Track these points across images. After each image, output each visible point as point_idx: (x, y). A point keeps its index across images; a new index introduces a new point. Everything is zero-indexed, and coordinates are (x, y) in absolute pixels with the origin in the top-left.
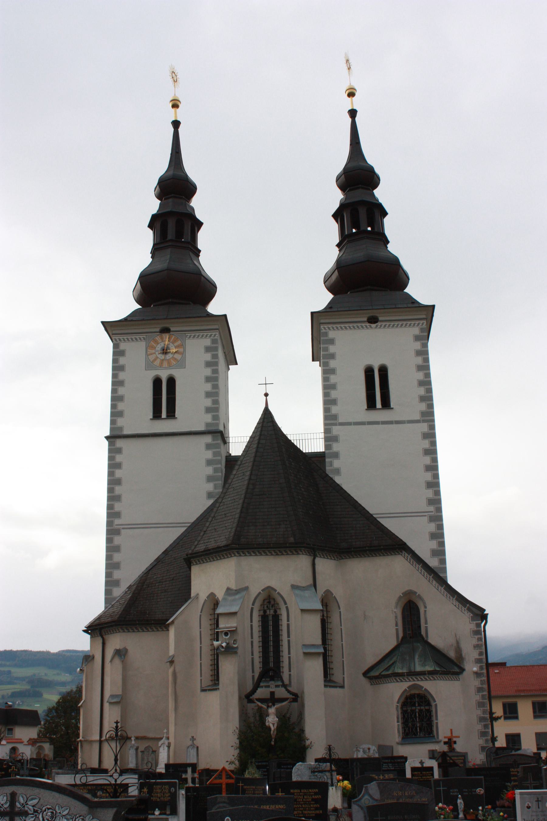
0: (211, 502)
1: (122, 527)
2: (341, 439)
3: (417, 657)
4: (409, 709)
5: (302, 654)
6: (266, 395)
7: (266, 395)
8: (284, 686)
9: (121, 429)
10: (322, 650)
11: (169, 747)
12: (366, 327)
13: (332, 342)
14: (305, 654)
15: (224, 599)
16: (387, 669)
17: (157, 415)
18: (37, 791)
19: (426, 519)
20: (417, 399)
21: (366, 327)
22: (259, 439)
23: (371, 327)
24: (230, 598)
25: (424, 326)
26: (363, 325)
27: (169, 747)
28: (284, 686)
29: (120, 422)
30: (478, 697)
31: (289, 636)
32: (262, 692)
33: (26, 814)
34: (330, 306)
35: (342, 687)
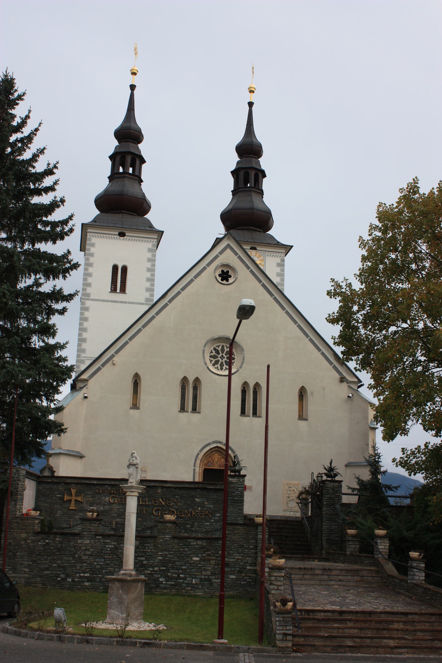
1: (86, 358)
12: (117, 238)
13: (93, 245)
21: (117, 238)
23: (120, 239)
26: (115, 237)
34: (95, 220)
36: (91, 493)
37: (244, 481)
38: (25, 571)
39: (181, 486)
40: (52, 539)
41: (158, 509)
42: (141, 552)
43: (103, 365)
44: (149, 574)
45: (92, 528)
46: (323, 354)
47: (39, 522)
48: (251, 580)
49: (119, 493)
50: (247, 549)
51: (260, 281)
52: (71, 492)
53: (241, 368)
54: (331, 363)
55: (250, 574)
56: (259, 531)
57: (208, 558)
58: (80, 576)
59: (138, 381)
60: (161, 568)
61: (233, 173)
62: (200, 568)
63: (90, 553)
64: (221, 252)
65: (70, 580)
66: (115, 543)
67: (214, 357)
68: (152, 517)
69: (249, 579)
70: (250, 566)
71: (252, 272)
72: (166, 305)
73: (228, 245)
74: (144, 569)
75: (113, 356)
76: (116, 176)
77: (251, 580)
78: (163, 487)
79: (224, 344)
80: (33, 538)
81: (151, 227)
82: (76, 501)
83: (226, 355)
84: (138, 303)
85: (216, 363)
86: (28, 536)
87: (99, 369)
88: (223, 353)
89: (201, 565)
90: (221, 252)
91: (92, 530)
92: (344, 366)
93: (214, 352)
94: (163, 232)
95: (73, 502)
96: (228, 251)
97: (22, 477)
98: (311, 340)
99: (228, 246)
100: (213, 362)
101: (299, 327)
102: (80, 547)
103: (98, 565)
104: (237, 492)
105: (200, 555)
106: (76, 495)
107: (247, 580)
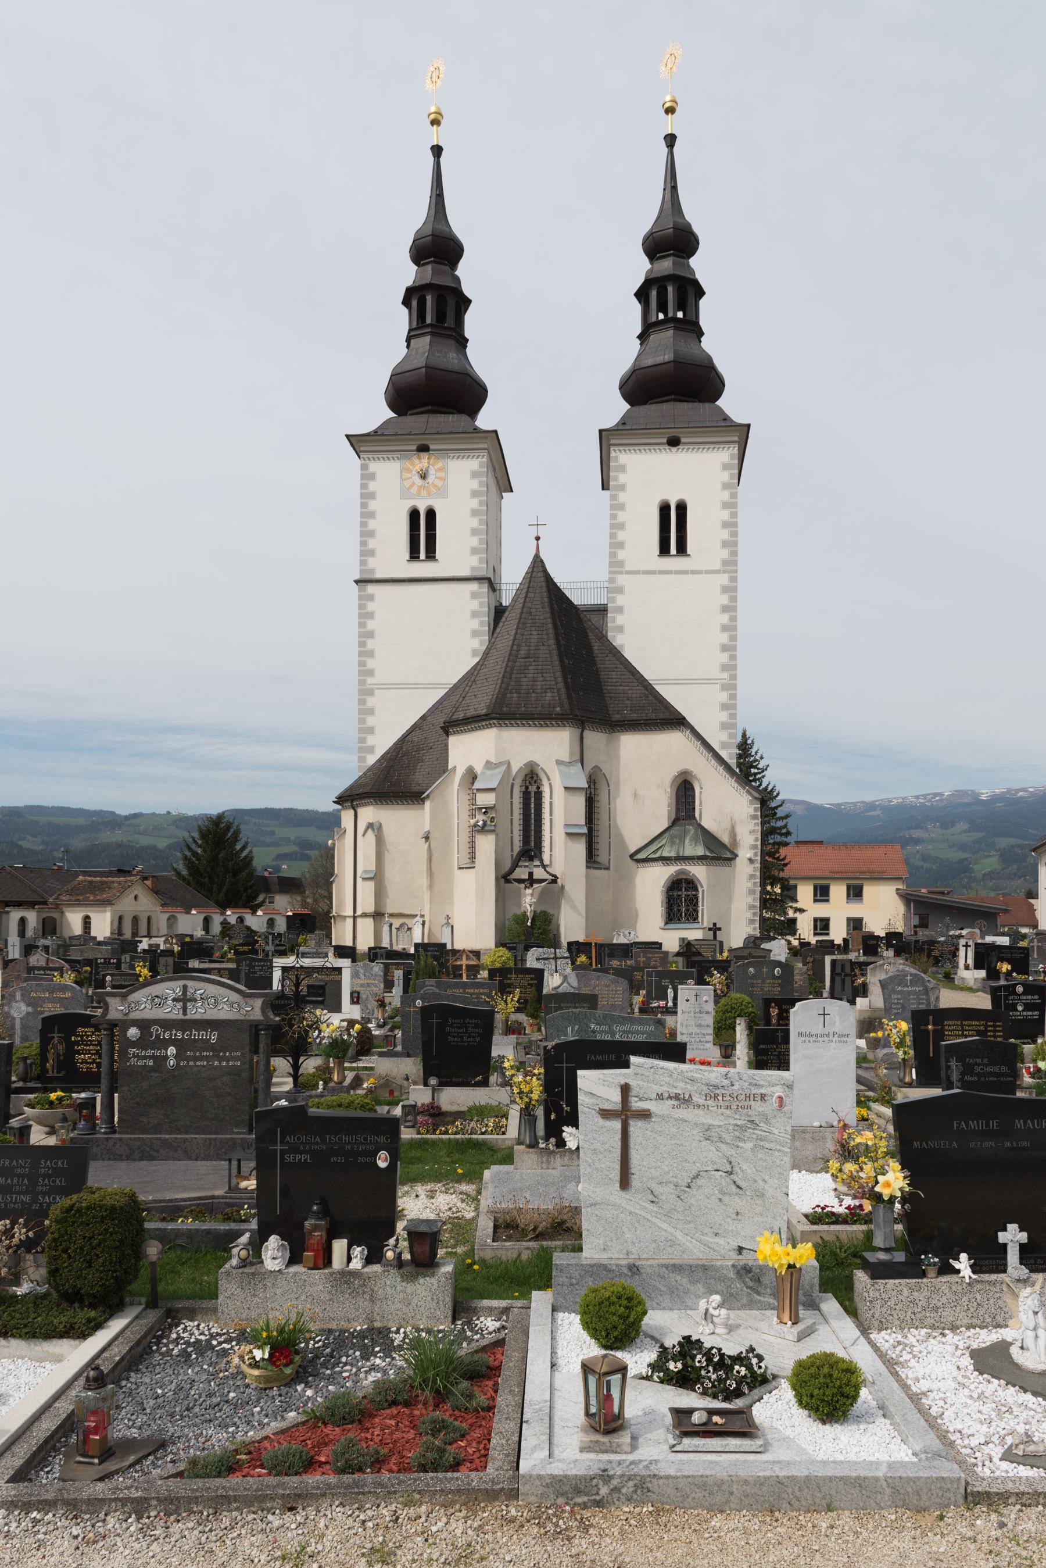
0: (477, 659)
2: (627, 590)
3: (687, 840)
4: (675, 893)
5: (563, 835)
6: (538, 538)
7: (538, 538)
8: (544, 867)
9: (373, 571)
10: (585, 830)
11: (423, 924)
14: (568, 834)
15: (483, 773)
16: (655, 852)
17: (414, 555)
18: (202, 984)
19: (717, 687)
20: (719, 544)
22: (527, 592)
24: (489, 772)
25: (736, 451)
27: (423, 924)
28: (544, 867)
29: (372, 563)
30: (749, 885)
31: (551, 815)
32: (521, 873)
33: (195, 1000)
34: (623, 422)
35: (608, 869)
81: (725, 419)
84: (708, 572)
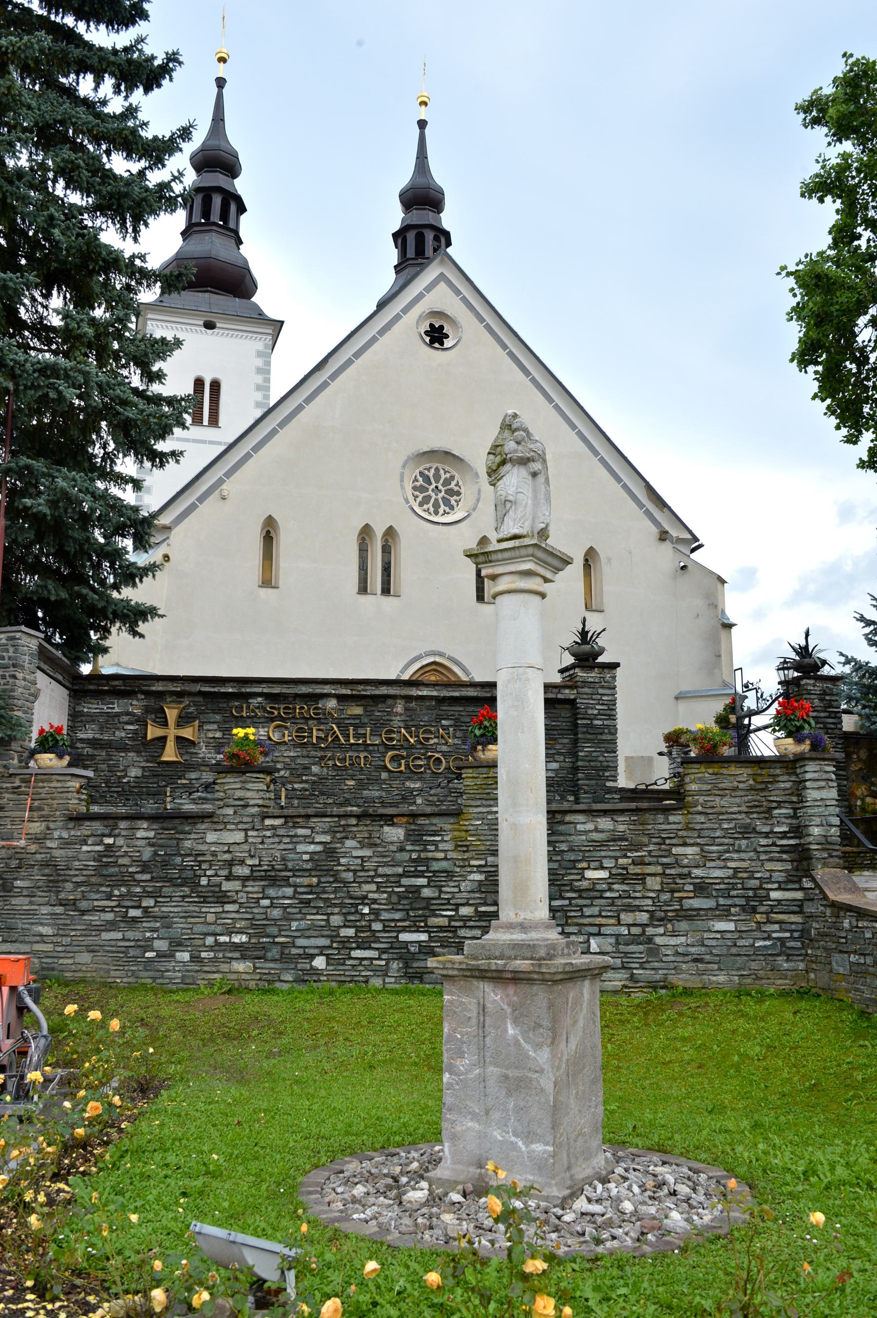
26: (198, 328)
36: (218, 717)
37: (614, 678)
38: (41, 935)
39: (456, 694)
40: (124, 833)
41: (397, 756)
42: (414, 861)
43: (202, 499)
44: (441, 928)
45: (249, 794)
46: (625, 487)
47: (81, 787)
48: (788, 935)
49: (294, 718)
50: (767, 835)
51: (504, 347)
52: (166, 718)
53: (474, 509)
54: (640, 505)
55: (781, 917)
56: (808, 776)
57: (637, 870)
58: (217, 943)
59: (273, 534)
60: (483, 909)
61: (395, 236)
62: (612, 905)
63: (246, 871)
64: (429, 288)
65: (185, 956)
66: (327, 838)
67: (422, 489)
68: (384, 775)
69: (782, 930)
70: (779, 889)
71: (488, 328)
72: (324, 385)
73: (442, 274)
74: (427, 913)
75: (220, 482)
76: (196, 229)
77: (788, 935)
78: (408, 698)
79: (440, 466)
80: (65, 835)
82: (179, 739)
83: (443, 485)
85: (426, 500)
86: (48, 828)
87: (192, 508)
88: (437, 481)
89: (616, 895)
90: (429, 288)
91: (252, 802)
92: (665, 510)
93: (421, 479)
94: (282, 322)
95: (170, 745)
96: (442, 285)
97: (27, 657)
98: (603, 461)
99: (442, 277)
100: (420, 499)
101: (580, 434)
102: (214, 854)
103: (272, 906)
104: (598, 707)
105: (608, 863)
106: (179, 725)
107: (775, 935)
